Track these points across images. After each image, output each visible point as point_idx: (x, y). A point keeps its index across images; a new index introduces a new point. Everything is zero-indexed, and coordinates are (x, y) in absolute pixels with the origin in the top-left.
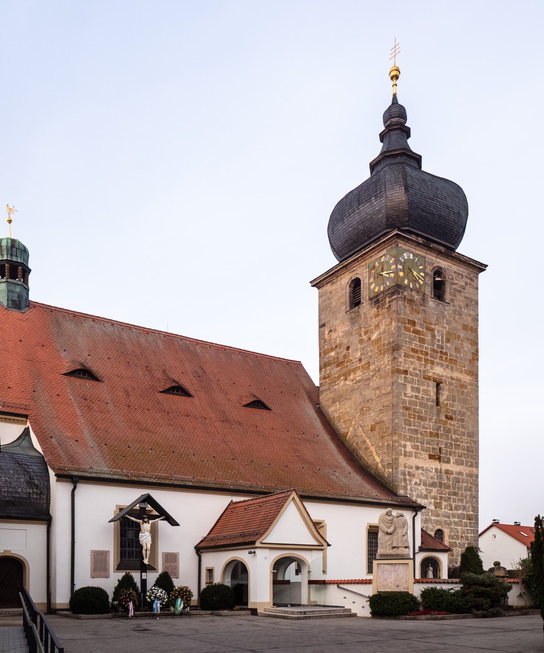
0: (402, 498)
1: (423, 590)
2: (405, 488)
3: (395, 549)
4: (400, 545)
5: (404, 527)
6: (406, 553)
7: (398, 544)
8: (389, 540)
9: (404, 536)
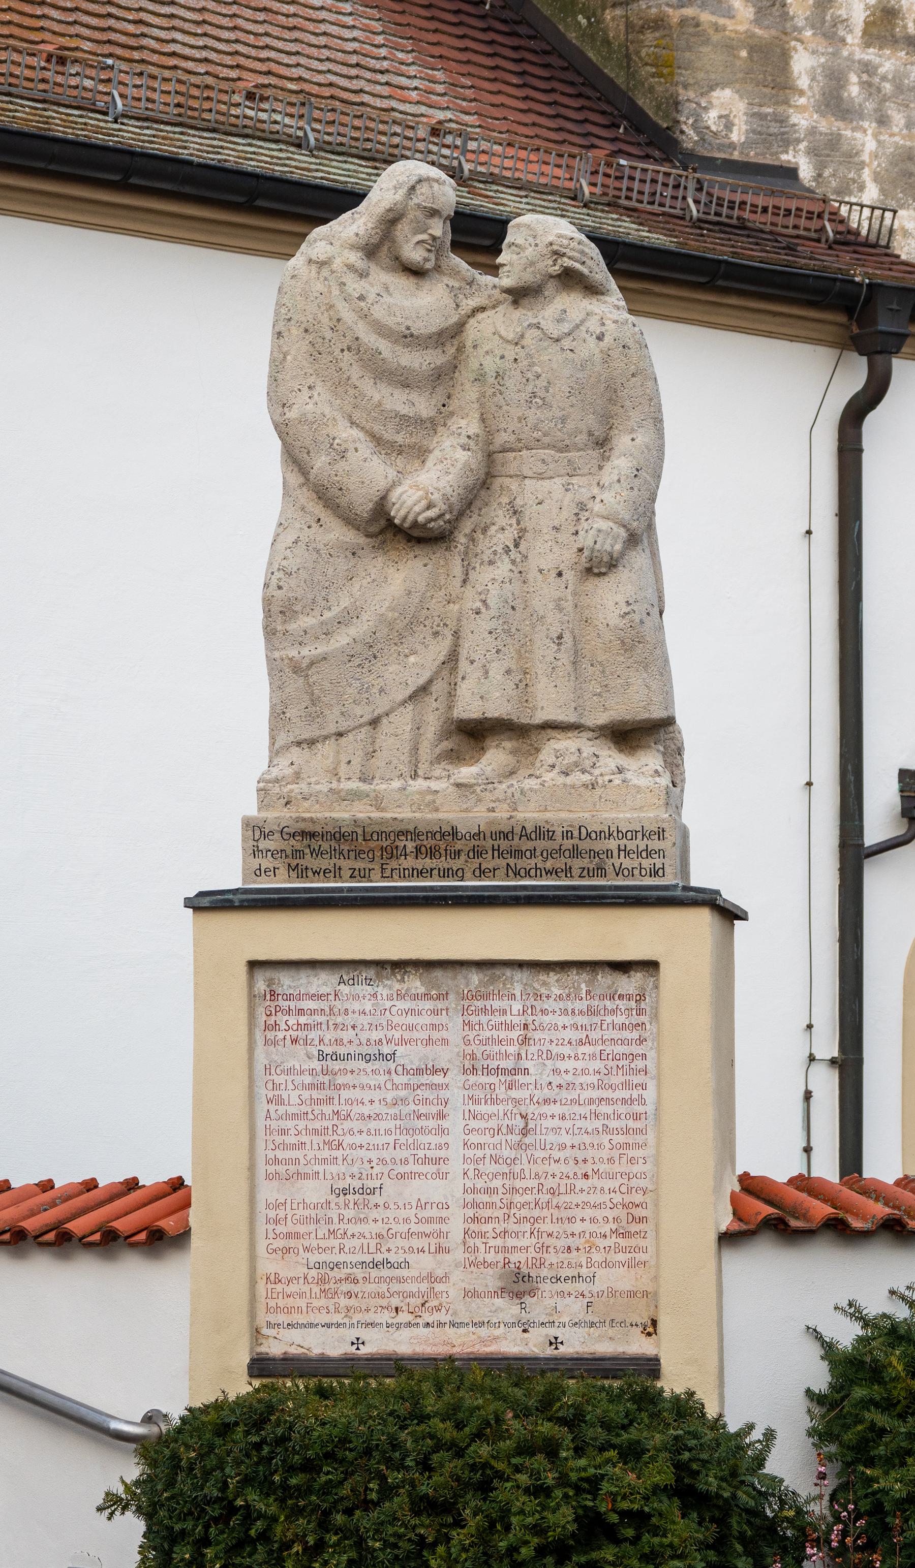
0: (723, 187)
1: (846, 1334)
2: (767, 69)
3: (496, 756)
4: (550, 704)
5: (602, 443)
6: (624, 816)
7: (524, 683)
8: (404, 627)
9: (598, 567)
